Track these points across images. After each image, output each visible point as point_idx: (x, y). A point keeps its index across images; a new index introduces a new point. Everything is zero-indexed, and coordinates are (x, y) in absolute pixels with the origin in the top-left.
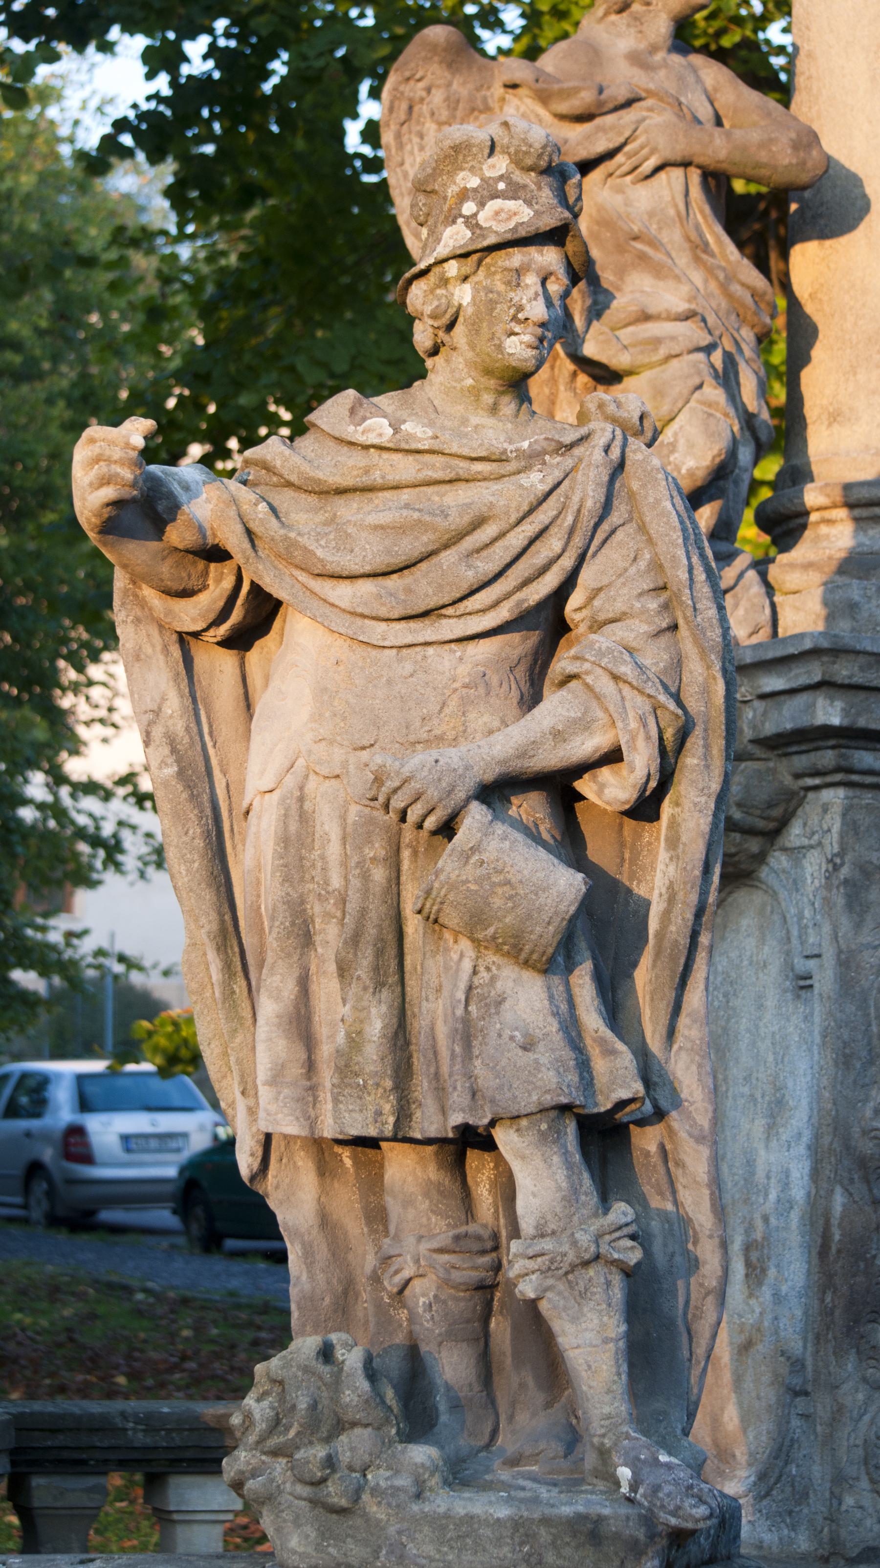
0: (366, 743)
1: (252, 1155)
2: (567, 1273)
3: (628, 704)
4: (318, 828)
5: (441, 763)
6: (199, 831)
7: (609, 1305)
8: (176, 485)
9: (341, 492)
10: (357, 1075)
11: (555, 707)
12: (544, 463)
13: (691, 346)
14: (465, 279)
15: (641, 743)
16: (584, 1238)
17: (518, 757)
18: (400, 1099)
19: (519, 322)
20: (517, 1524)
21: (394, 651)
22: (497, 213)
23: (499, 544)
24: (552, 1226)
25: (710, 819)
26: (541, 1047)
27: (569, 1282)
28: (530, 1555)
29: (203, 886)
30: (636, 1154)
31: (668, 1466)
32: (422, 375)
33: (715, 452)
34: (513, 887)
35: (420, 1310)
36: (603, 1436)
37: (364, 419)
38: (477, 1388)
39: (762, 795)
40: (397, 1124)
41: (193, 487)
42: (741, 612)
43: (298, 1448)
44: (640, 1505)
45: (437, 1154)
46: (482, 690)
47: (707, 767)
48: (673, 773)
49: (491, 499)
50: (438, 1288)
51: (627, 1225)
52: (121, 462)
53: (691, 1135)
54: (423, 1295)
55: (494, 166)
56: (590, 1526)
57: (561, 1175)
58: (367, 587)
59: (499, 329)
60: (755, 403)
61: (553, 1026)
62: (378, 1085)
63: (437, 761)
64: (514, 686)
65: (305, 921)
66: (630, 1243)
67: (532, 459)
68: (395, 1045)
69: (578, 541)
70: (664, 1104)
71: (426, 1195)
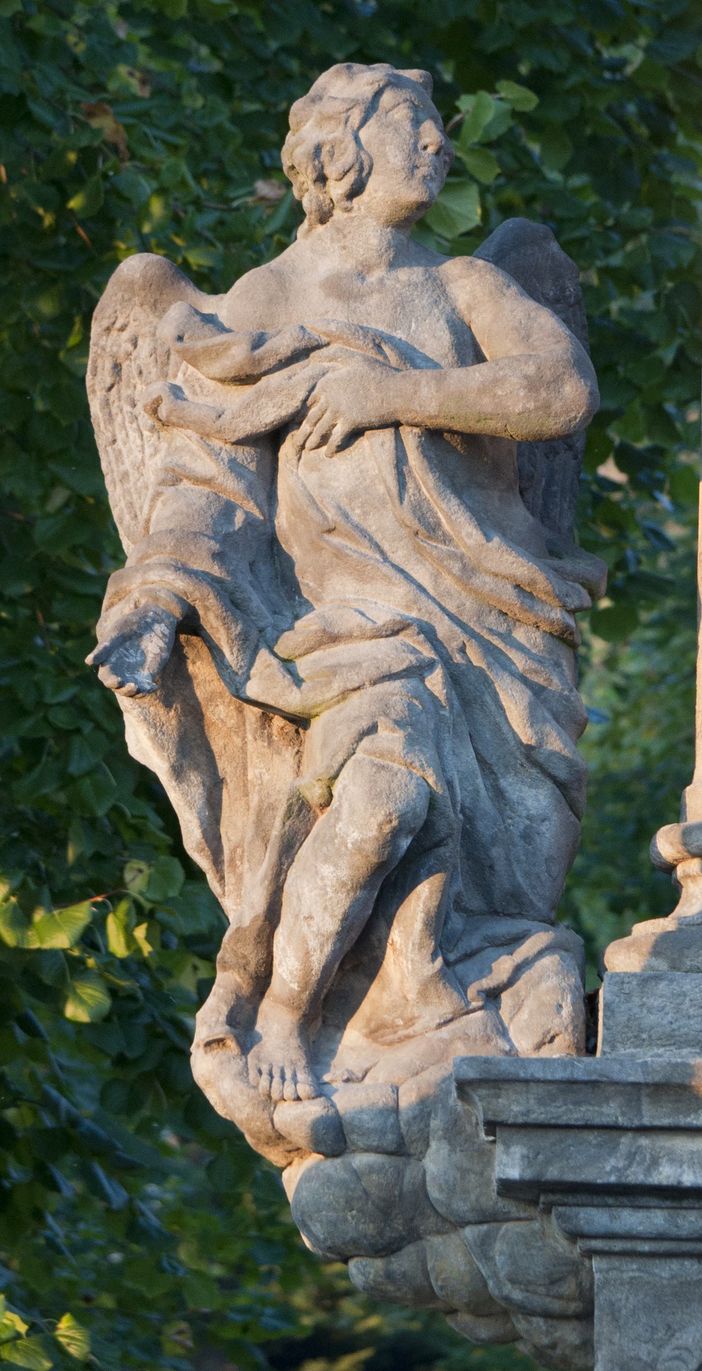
13: (375, 674)
33: (380, 818)
39: (537, 1266)
42: (524, 1015)
60: (529, 731)
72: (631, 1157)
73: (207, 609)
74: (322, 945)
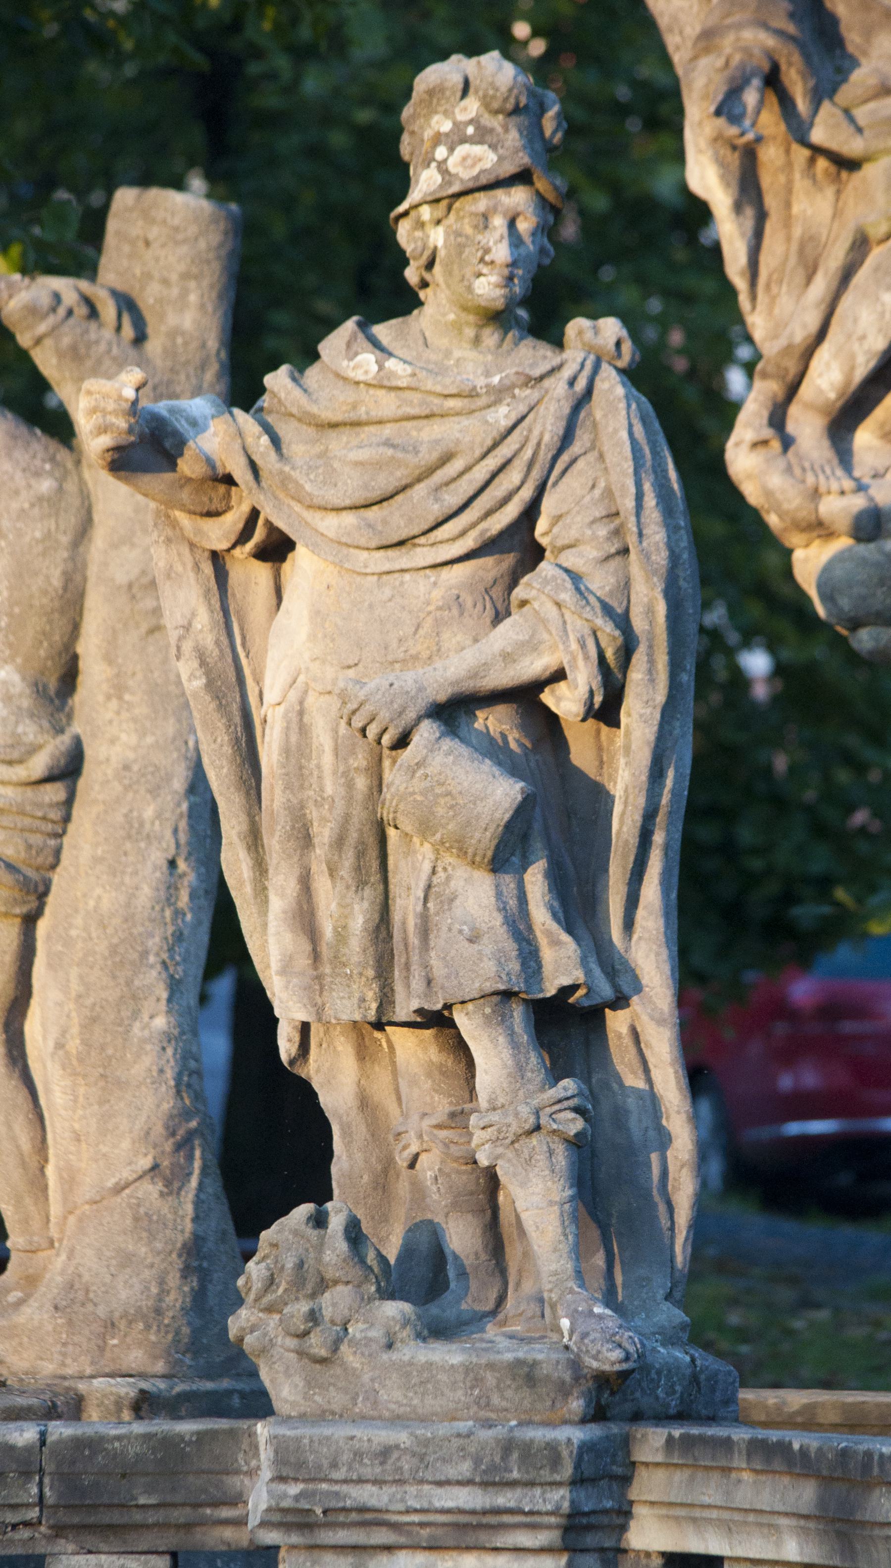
0: (351, 663)
1: (290, 1040)
2: (513, 1143)
3: (569, 627)
4: (314, 740)
5: (395, 686)
6: (226, 738)
7: (553, 1171)
8: (183, 422)
9: (334, 426)
10: (345, 965)
11: (509, 632)
12: (514, 397)
14: (438, 222)
15: (581, 662)
16: (525, 1111)
17: (470, 678)
18: (382, 988)
19: (486, 264)
20: (468, 1369)
21: (375, 577)
22: (464, 159)
23: (466, 477)
24: (501, 1100)
25: (656, 728)
26: (485, 940)
27: (516, 1150)
28: (480, 1397)
29: (232, 789)
30: (611, 1035)
31: (600, 1317)
32: (419, 303)
34: (453, 798)
35: (429, 1183)
36: (551, 1291)
37: (356, 354)
38: (484, 1257)
40: (380, 1009)
41: (200, 421)
43: (286, 1304)
44: (572, 1351)
45: (436, 1037)
46: (455, 611)
47: (652, 681)
48: (623, 686)
49: (458, 435)
50: (442, 1162)
51: (567, 1099)
52: (115, 412)
53: (652, 1018)
54: (430, 1169)
55: (465, 109)
56: (526, 1369)
57: (506, 1054)
58: (349, 519)
59: (468, 272)
61: (498, 920)
62: (361, 974)
63: (391, 685)
64: (488, 605)
65: (304, 825)
66: (571, 1115)
67: (499, 394)
68: (377, 937)
69: (536, 474)
70: (626, 989)
71: (429, 1075)
73: (790, 64)
74: (868, 361)
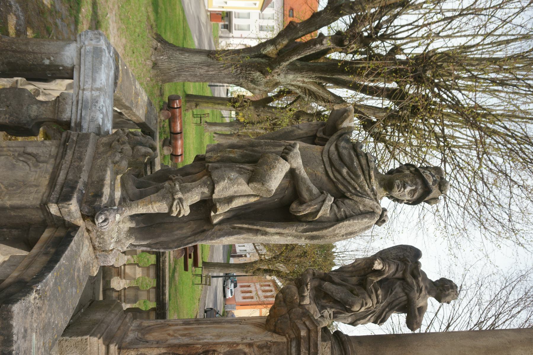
72: (305, 353)
